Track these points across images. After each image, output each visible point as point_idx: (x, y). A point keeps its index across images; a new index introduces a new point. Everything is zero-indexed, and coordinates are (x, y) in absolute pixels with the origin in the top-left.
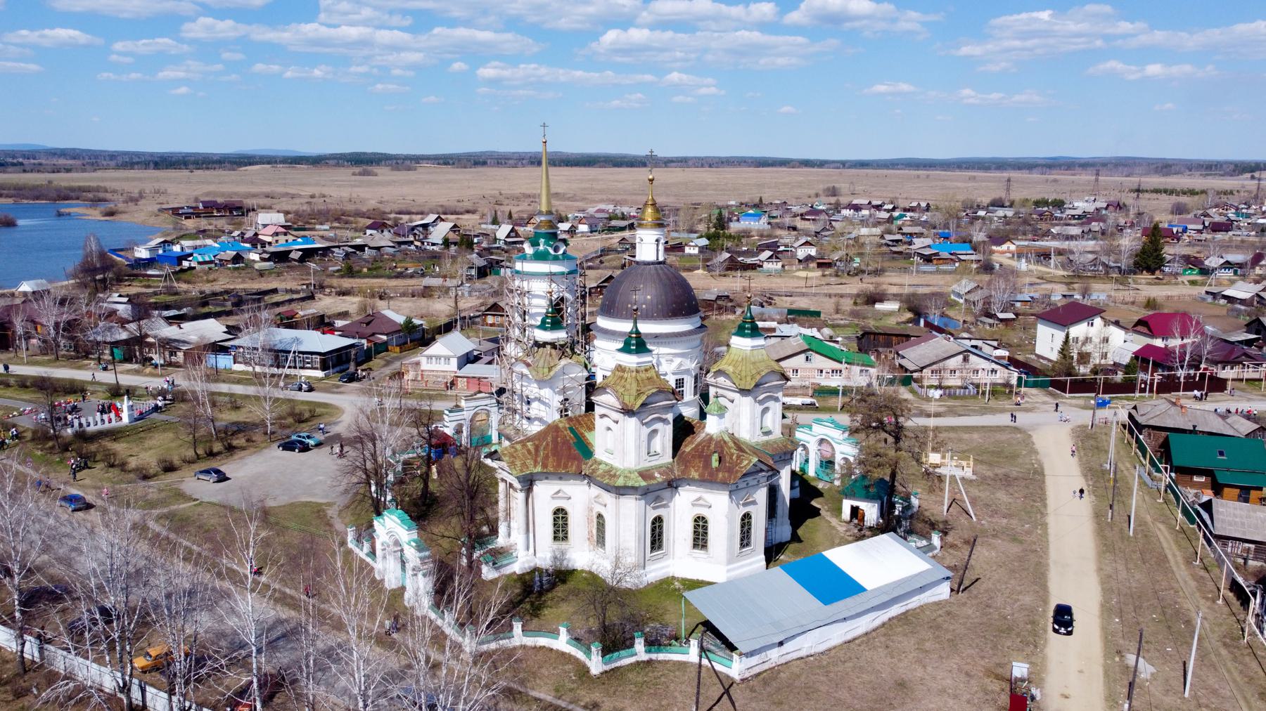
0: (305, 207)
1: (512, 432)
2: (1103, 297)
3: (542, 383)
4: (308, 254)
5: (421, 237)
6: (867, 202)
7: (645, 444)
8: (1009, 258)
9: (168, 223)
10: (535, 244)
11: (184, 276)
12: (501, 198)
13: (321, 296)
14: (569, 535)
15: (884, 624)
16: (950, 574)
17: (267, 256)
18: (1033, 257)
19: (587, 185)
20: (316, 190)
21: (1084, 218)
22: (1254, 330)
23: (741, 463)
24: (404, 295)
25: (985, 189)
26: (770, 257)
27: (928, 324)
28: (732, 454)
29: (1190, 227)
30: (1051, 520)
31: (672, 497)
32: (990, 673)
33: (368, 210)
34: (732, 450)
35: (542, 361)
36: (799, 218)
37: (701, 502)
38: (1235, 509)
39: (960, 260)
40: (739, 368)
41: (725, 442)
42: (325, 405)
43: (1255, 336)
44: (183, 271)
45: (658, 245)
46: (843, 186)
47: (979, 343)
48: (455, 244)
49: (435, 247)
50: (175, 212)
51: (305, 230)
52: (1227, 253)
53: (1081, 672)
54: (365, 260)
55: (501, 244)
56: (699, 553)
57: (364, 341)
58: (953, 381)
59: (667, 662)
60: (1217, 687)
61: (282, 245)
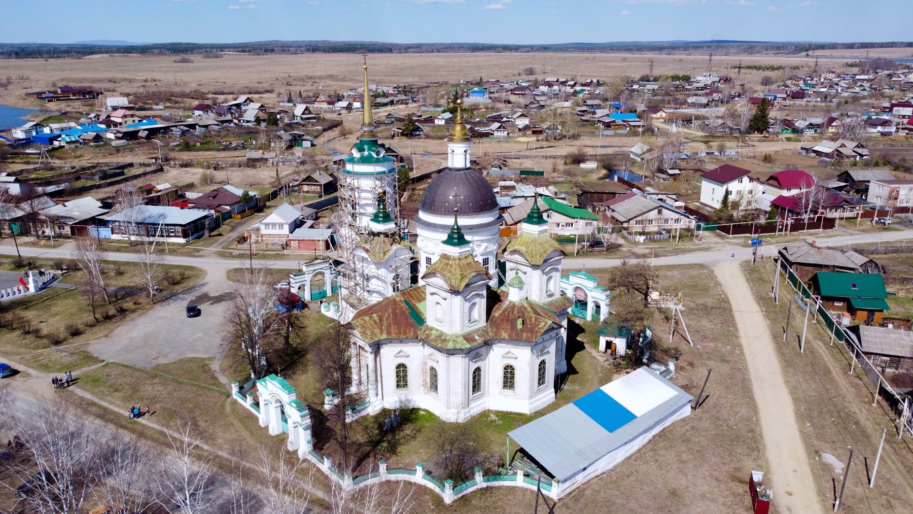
0: (141, 90)
1: (356, 302)
2: (733, 153)
3: (379, 265)
4: (152, 133)
5: (237, 115)
6: (555, 80)
7: (467, 315)
8: (662, 123)
9: (35, 106)
10: (361, 150)
11: (56, 153)
12: (290, 80)
13: (168, 168)
14: (409, 383)
15: (650, 441)
16: (691, 398)
17: (120, 135)
18: (680, 122)
19: (351, 68)
20: (149, 76)
21: (708, 89)
22: (843, 180)
23: (539, 325)
24: (232, 165)
25: (635, 66)
26: (499, 128)
27: (620, 179)
28: (531, 318)
29: (778, 96)
30: (744, 341)
31: (488, 353)
32: (734, 478)
33: (191, 92)
34: (531, 314)
35: (378, 246)
36: (510, 93)
37: (509, 355)
38: (875, 332)
39: (630, 126)
40: (530, 248)
41: (525, 308)
42: (191, 268)
43: (843, 184)
44: (54, 149)
45: (465, 155)
46: (537, 67)
47: (664, 197)
48: (264, 121)
49: (249, 124)
50: (39, 95)
51: (144, 109)
52: (810, 117)
53: (795, 471)
54: (197, 136)
55: (298, 120)
56: (508, 392)
57: (213, 212)
58: (652, 228)
59: (499, 488)
60: (888, 476)
61: (129, 126)
